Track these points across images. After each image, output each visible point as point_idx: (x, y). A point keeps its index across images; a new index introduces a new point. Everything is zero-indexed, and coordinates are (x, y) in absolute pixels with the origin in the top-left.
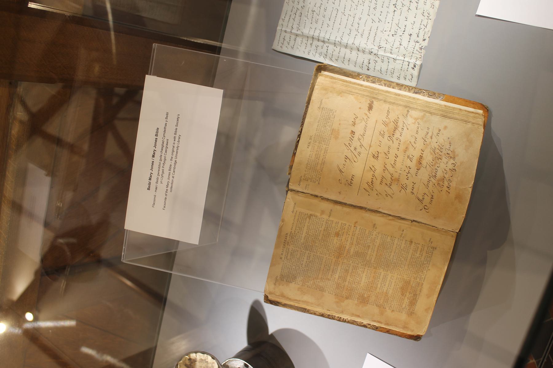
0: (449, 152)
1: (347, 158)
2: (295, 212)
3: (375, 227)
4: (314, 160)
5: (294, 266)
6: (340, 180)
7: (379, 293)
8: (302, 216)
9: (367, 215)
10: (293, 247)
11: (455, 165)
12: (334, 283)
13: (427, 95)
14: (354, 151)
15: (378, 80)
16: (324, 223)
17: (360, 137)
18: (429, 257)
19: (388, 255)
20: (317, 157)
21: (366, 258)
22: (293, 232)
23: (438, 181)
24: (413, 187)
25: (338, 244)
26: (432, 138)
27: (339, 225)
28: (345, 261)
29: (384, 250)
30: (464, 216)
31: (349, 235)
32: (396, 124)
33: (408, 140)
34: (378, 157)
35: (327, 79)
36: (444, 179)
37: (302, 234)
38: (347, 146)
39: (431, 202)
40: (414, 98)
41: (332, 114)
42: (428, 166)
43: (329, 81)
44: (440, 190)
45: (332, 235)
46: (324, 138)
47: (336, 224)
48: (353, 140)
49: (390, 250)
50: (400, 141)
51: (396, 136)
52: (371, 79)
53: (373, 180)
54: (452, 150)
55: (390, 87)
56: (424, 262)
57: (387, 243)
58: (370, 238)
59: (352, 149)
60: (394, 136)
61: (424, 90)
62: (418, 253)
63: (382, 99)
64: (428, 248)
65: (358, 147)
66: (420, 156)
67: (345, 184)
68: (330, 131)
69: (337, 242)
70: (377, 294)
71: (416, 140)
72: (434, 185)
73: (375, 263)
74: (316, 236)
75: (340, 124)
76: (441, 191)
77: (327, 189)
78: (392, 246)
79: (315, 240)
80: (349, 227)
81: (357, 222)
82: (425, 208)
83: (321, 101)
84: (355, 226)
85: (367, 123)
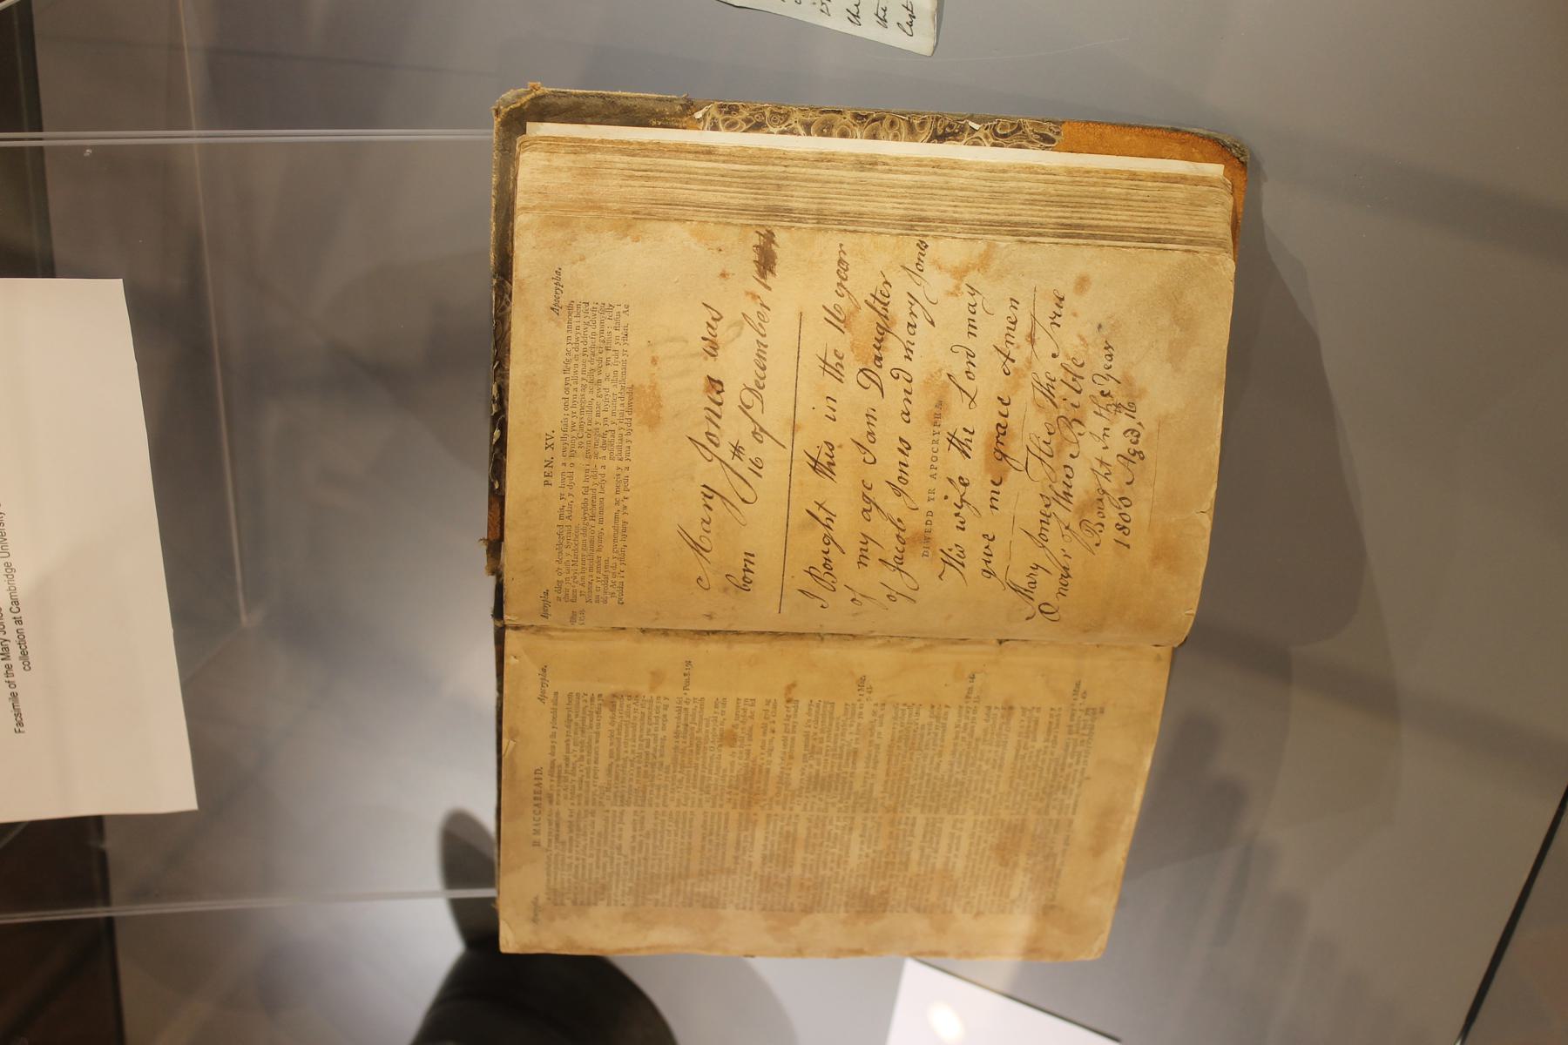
0: (1110, 386)
1: (710, 494)
2: (551, 696)
3: (866, 685)
4: (581, 526)
5: (591, 856)
6: (700, 578)
7: (918, 875)
8: (582, 704)
9: (827, 653)
10: (573, 804)
11: (1138, 436)
12: (751, 878)
13: (987, 137)
14: (735, 463)
15: (772, 112)
16: (671, 713)
17: (748, 398)
18: (1083, 741)
19: (931, 763)
20: (589, 512)
21: (851, 788)
22: (560, 761)
23: (1082, 509)
24: (987, 551)
25: (737, 767)
26: (1032, 342)
27: (731, 707)
28: (777, 809)
29: (912, 754)
30: (1194, 612)
31: (773, 732)
32: (883, 312)
33: (940, 371)
34: (833, 464)
35: (562, 160)
36: (1101, 500)
37: (596, 762)
38: (703, 446)
39: (1062, 591)
40: (937, 165)
41: (612, 323)
42: (1033, 461)
43: (570, 169)
44: (1092, 545)
45: (710, 744)
46: (601, 431)
47: (716, 707)
48: (719, 417)
49: (934, 749)
50: (910, 382)
51: (888, 364)
52: (745, 114)
53: (829, 556)
54: (1117, 375)
55: (829, 135)
56: (1065, 758)
57: (919, 731)
58: (854, 729)
59: (725, 452)
60: (880, 367)
61: (971, 118)
62: (1041, 737)
63: (806, 211)
64: (1073, 715)
65: (747, 442)
66: (999, 425)
67: (725, 590)
68: (622, 398)
69: (732, 764)
70: (911, 879)
71: (972, 360)
72: (1067, 528)
73: (887, 795)
74: (651, 757)
75: (654, 361)
76: (1097, 545)
77: (657, 613)
78: (940, 736)
79: (649, 769)
80: (767, 708)
81: (794, 685)
82: (1042, 612)
83: (555, 276)
84: (789, 701)
85: (762, 331)
